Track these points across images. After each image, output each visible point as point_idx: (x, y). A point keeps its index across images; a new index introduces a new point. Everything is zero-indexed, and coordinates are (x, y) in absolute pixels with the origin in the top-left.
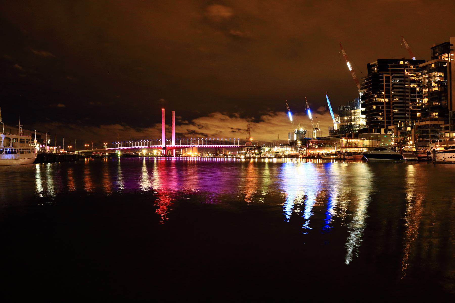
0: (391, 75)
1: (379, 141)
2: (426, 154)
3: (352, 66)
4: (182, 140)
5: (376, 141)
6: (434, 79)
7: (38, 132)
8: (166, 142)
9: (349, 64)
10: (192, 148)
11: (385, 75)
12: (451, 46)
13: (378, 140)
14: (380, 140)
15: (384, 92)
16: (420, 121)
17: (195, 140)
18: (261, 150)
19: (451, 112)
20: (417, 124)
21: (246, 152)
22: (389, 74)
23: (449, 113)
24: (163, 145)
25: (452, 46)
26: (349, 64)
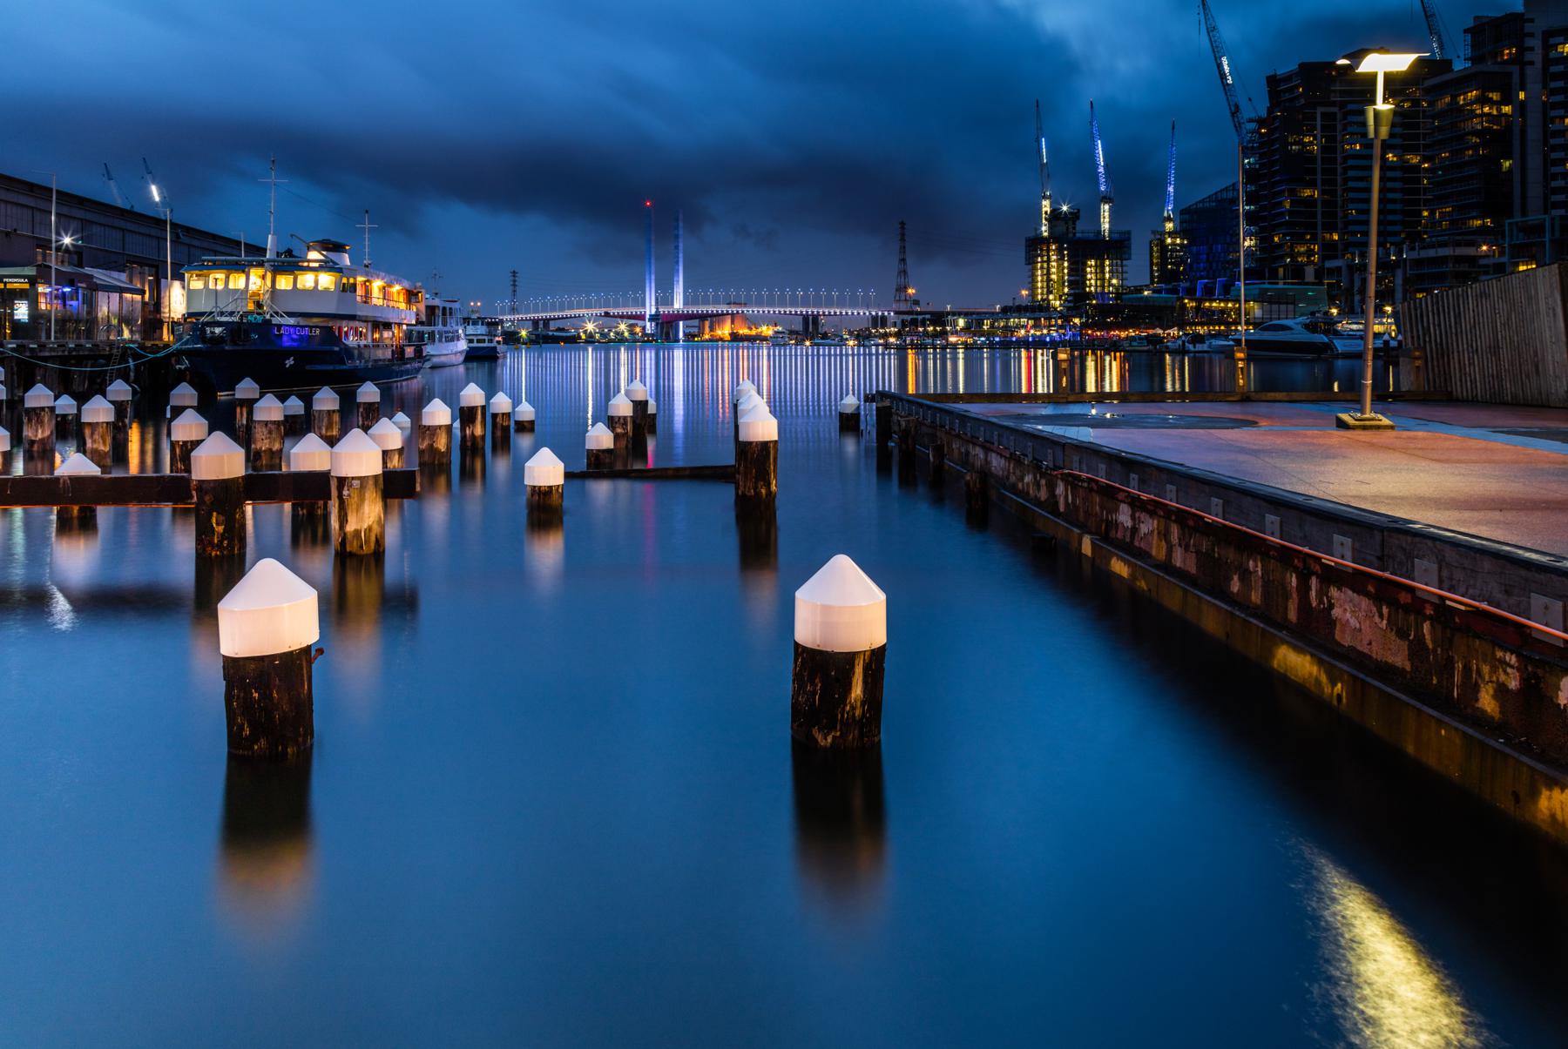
0: (1340, 110)
1: (1291, 307)
2: (1097, 387)
3: (161, 194)
4: (706, 293)
5: (1283, 307)
6: (1470, 124)
7: (1360, 123)
8: (657, 299)
9: (154, 190)
10: (730, 316)
11: (1320, 110)
12: (1526, 24)
13: (1287, 303)
14: (1294, 303)
15: (327, 280)
16: (1420, 249)
17: (765, 292)
18: (943, 324)
19: (1510, 224)
20: (1414, 255)
21: (899, 331)
22: (1333, 104)
23: (1507, 225)
24: (650, 309)
25: (1531, 24)
26: (154, 190)
